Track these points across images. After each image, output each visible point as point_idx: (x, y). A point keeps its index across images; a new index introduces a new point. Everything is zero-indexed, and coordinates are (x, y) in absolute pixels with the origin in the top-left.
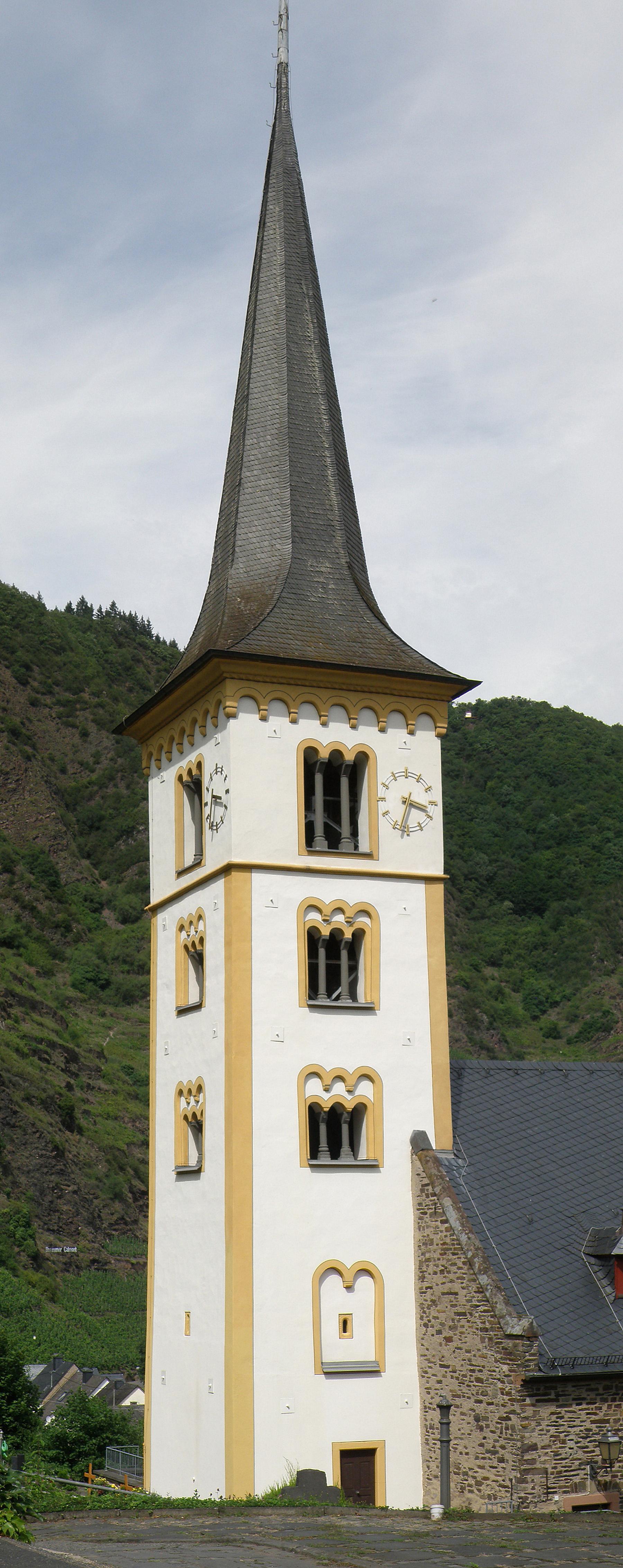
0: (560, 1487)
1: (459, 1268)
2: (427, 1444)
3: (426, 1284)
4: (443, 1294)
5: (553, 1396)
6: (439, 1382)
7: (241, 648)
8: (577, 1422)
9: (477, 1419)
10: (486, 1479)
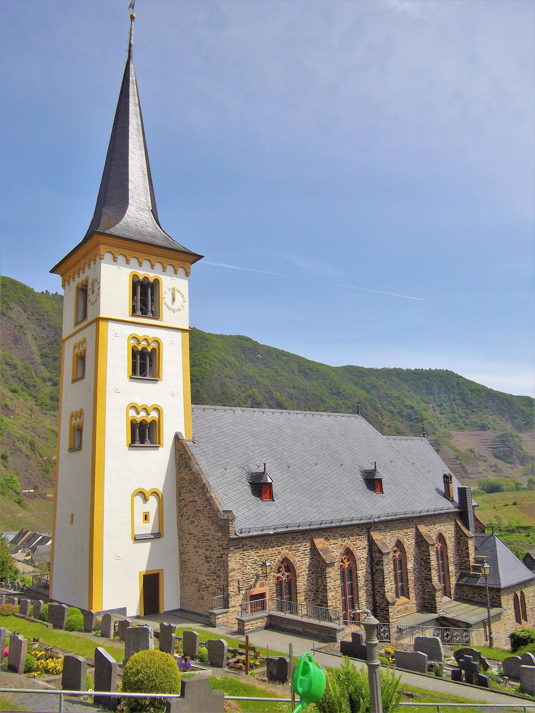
0: (245, 587)
1: (198, 490)
2: (182, 569)
3: (181, 498)
4: (190, 502)
5: (241, 546)
6: (188, 541)
7: (107, 232)
8: (251, 557)
9: (206, 558)
10: (211, 585)
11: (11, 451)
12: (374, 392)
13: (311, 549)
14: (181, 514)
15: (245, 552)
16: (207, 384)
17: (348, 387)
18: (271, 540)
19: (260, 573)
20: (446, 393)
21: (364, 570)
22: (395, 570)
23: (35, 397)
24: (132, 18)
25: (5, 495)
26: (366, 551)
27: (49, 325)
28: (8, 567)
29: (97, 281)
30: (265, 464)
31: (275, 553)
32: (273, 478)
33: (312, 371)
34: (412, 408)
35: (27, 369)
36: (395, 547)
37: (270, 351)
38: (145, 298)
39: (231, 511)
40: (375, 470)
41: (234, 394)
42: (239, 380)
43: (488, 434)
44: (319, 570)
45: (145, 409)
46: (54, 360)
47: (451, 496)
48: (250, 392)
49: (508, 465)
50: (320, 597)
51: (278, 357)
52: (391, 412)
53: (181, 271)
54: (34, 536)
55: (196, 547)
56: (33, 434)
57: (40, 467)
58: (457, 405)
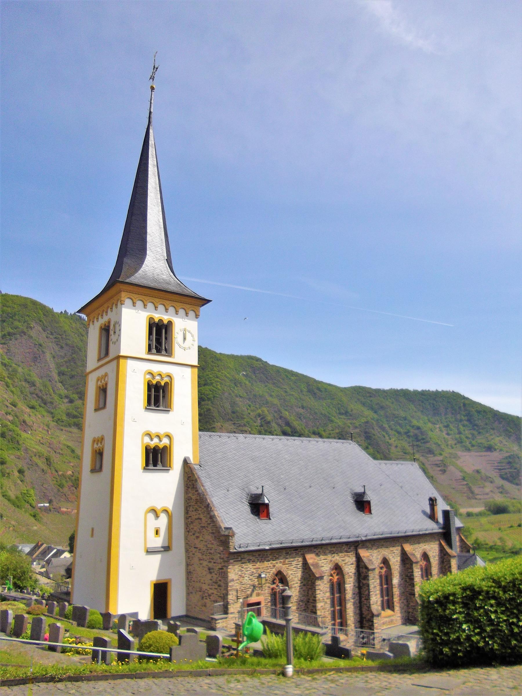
4: (196, 519)
5: (239, 559)
6: (193, 554)
7: (127, 281)
8: (249, 569)
9: (209, 569)
10: (213, 593)
11: (28, 466)
12: (382, 413)
13: (303, 564)
14: (188, 530)
15: (243, 565)
16: (218, 403)
17: (355, 407)
18: (267, 555)
19: (257, 583)
20: (452, 414)
21: (352, 584)
22: (381, 585)
23: (52, 413)
24: (152, 88)
25: (21, 509)
26: (354, 566)
27: (67, 345)
28: (28, 577)
29: (118, 323)
30: (263, 486)
31: (270, 566)
32: (270, 499)
33: (320, 391)
34: (418, 428)
35: (45, 386)
36: (381, 563)
37: (279, 371)
38: (159, 336)
39: (231, 528)
40: (364, 493)
41: (244, 413)
42: (249, 399)
43: (495, 456)
44: (310, 582)
45: (158, 436)
46: (71, 378)
47: (436, 518)
48: (260, 411)
49: (514, 486)
50: (311, 607)
51: (287, 377)
52: (399, 433)
53: (192, 314)
54: (50, 549)
55: (201, 560)
56: (49, 449)
57: (55, 482)
58: (464, 426)
